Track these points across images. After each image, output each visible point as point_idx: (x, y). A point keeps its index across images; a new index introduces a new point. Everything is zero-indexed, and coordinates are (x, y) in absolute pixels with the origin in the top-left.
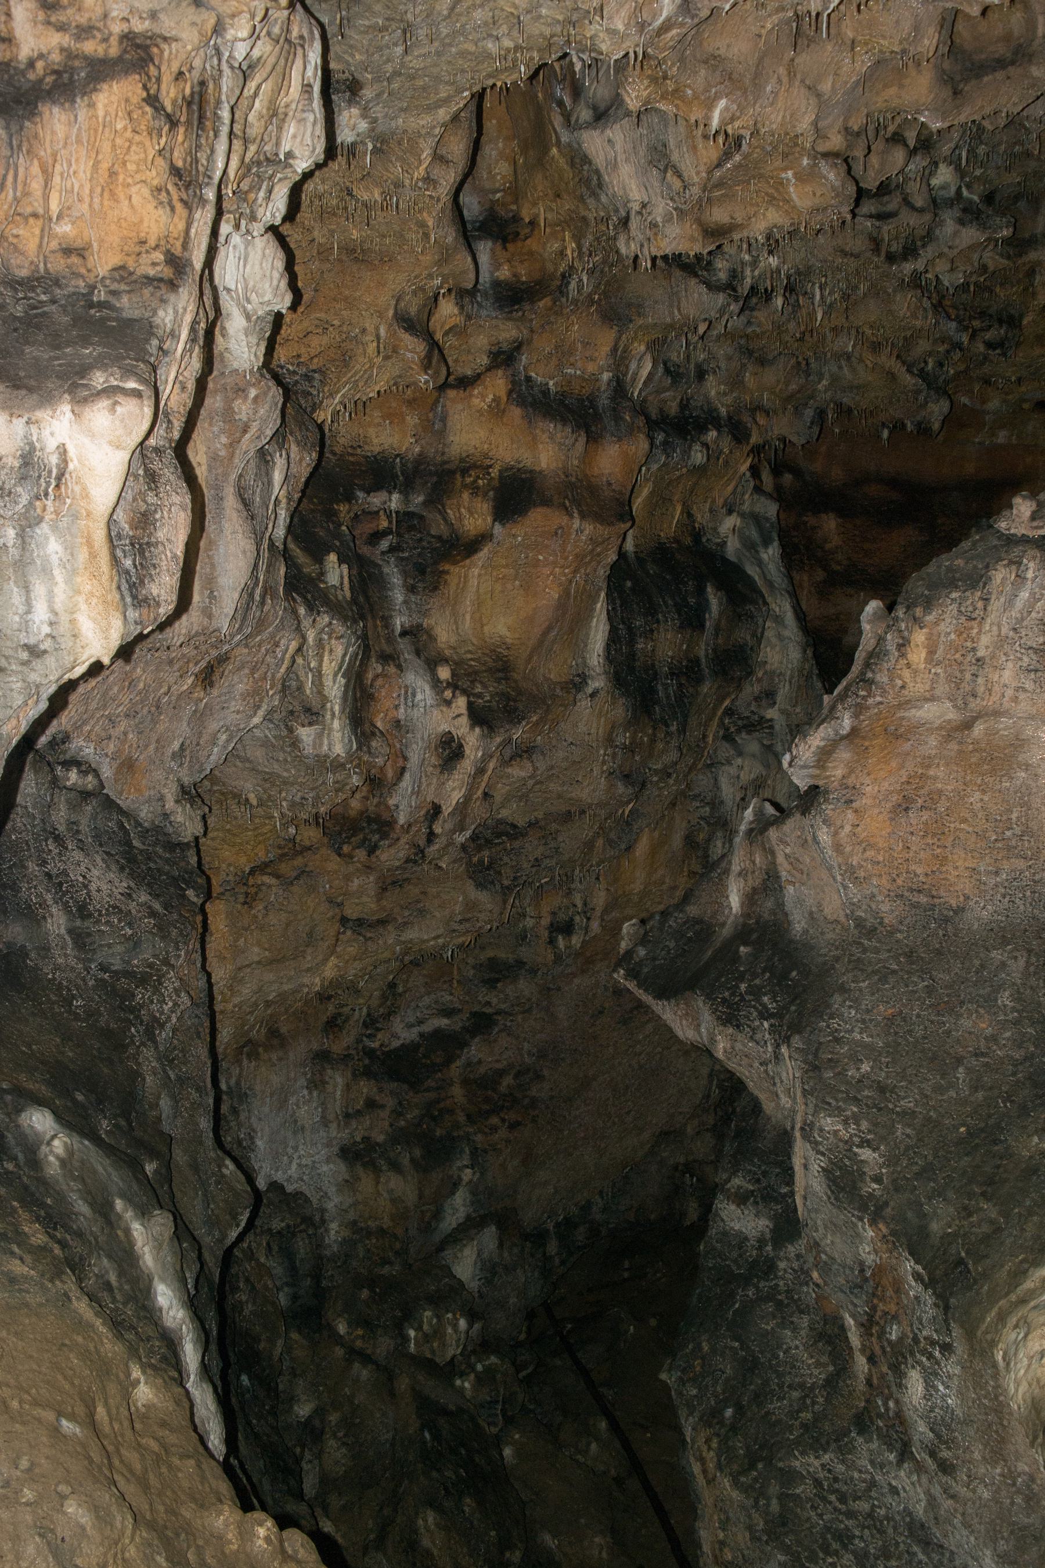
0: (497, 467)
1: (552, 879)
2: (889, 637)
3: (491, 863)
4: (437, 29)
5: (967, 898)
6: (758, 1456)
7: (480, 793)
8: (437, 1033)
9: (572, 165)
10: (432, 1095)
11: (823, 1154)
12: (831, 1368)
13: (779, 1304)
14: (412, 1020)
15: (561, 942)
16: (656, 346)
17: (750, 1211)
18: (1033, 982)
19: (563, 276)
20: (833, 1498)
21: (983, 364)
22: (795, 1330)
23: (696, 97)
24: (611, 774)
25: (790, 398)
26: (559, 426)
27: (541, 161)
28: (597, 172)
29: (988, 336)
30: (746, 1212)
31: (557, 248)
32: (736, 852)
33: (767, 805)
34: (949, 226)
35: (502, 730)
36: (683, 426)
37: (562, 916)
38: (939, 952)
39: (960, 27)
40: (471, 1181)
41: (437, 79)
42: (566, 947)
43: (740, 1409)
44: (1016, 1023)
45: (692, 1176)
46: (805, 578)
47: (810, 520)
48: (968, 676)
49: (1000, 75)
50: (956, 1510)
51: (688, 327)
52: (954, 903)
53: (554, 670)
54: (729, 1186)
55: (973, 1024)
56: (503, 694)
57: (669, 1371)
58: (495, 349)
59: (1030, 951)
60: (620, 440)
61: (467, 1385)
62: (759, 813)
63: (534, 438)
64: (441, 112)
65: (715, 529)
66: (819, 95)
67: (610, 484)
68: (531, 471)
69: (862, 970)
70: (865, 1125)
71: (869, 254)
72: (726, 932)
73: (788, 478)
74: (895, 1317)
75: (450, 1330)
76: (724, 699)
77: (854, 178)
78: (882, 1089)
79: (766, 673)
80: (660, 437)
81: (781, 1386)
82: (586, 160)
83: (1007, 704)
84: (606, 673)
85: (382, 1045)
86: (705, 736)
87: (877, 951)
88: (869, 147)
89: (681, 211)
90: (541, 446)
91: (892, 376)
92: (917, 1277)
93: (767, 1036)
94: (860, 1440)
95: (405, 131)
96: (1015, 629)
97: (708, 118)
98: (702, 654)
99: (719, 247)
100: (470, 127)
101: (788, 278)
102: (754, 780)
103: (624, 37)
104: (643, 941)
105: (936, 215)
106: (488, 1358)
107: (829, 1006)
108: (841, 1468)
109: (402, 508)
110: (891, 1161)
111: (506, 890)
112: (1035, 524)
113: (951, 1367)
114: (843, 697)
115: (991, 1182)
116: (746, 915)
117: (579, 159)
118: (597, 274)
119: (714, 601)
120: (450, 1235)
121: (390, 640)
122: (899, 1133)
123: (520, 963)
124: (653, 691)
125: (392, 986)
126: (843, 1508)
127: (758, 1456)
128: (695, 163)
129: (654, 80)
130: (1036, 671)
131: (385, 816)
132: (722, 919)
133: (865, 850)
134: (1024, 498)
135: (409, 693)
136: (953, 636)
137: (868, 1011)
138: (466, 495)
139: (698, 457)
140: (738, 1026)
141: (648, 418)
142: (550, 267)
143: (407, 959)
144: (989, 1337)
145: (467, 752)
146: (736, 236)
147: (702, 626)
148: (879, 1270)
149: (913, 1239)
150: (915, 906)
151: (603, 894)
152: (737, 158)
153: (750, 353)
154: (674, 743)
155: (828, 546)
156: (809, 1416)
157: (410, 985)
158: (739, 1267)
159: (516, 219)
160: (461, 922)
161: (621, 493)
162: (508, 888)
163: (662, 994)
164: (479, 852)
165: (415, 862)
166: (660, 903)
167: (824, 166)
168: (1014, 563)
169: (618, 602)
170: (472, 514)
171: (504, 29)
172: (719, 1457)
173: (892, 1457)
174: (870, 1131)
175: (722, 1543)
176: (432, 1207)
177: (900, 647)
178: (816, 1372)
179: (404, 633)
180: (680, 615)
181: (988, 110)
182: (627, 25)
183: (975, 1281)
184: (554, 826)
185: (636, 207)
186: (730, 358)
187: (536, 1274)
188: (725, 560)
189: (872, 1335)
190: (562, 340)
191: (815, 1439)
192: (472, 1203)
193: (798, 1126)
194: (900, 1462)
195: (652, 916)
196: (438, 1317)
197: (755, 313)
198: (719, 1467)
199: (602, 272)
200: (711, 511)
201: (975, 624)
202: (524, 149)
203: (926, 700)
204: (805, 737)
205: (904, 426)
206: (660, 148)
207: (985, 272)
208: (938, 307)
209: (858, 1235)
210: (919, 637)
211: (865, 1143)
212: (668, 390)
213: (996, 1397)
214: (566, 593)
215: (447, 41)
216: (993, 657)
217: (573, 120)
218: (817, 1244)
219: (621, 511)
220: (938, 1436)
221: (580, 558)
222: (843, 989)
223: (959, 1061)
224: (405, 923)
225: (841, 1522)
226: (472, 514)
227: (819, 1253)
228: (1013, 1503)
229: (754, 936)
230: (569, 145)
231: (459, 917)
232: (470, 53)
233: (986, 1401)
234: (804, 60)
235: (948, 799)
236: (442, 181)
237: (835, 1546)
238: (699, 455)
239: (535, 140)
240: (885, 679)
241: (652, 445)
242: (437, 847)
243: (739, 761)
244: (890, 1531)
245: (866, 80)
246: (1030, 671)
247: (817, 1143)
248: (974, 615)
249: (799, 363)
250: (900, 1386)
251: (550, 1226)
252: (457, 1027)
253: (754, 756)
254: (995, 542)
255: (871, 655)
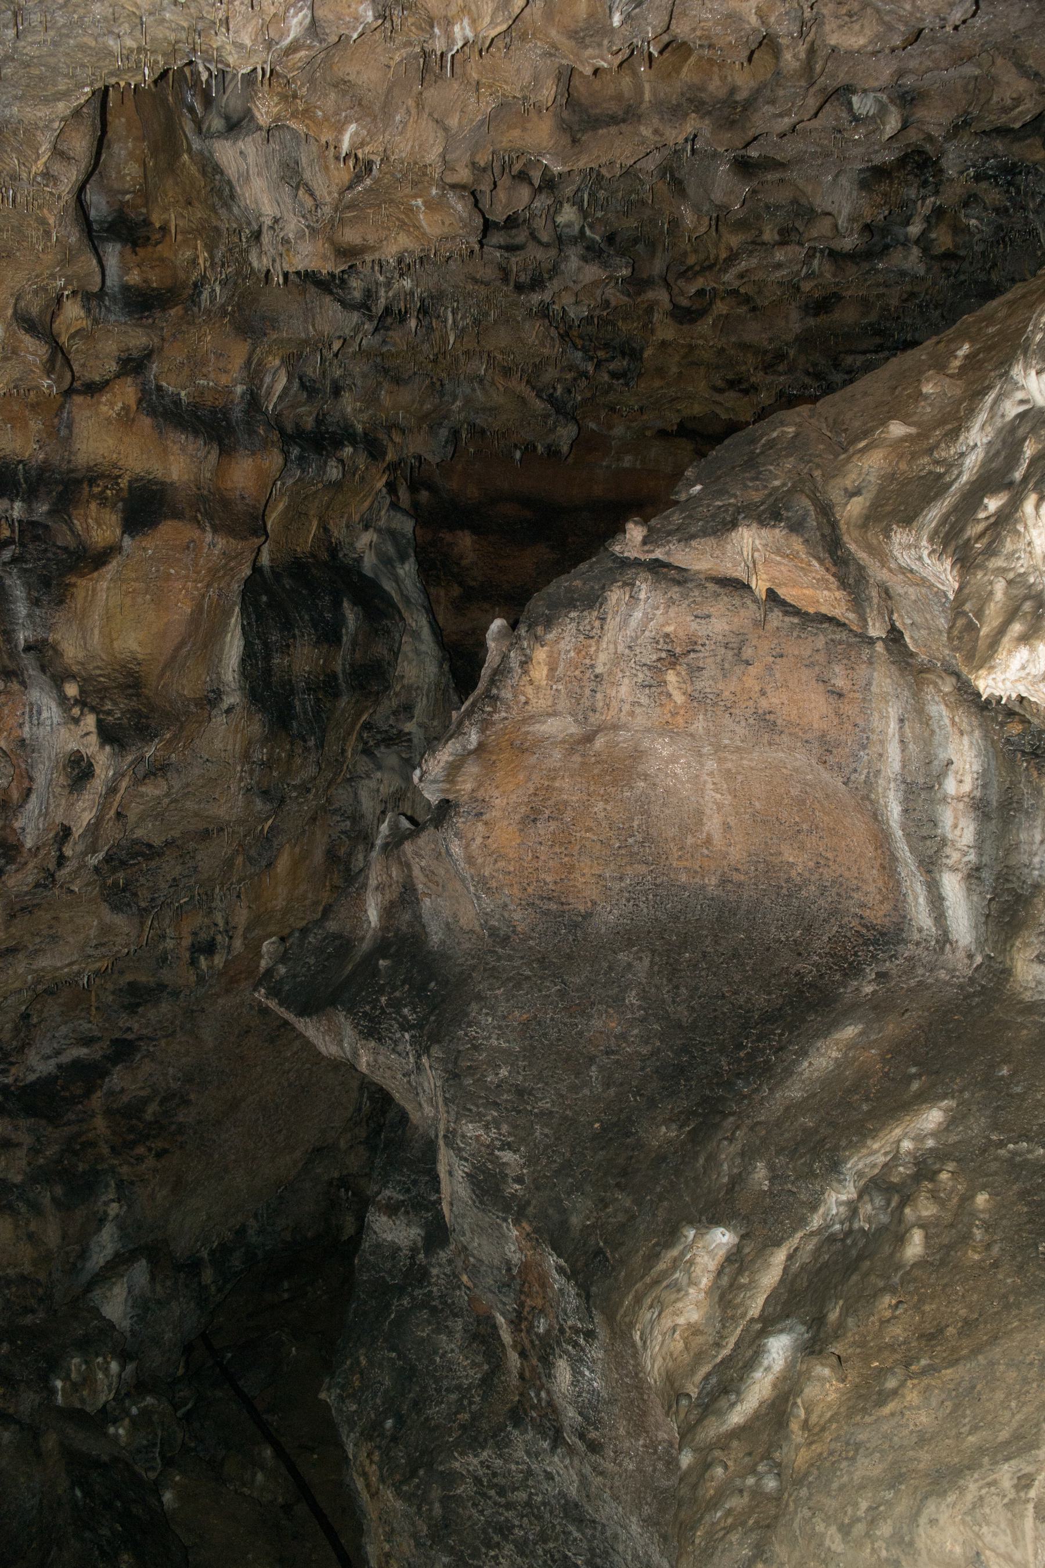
0: (127, 478)
1: (192, 898)
2: (512, 654)
3: (126, 885)
4: (53, 18)
5: (594, 903)
6: (417, 1465)
7: (112, 813)
8: (76, 1063)
9: (204, 173)
10: (74, 1128)
11: (466, 1160)
12: (486, 1367)
13: (434, 1310)
14: (49, 1051)
15: (203, 962)
16: (292, 361)
17: (401, 1220)
18: (657, 980)
19: (195, 285)
20: (492, 1493)
21: (607, 392)
22: (450, 1333)
23: (326, 119)
24: (248, 790)
25: (427, 415)
26: (191, 438)
27: (172, 167)
28: (229, 183)
29: (612, 366)
30: (398, 1222)
31: (189, 256)
32: (373, 867)
33: (402, 818)
34: (574, 262)
35: (134, 748)
36: (318, 441)
37: (203, 936)
38: (569, 957)
39: (576, 81)
40: (117, 1216)
41: (55, 70)
42: (210, 968)
43: (400, 1420)
44: (643, 1020)
45: (347, 1191)
46: (442, 593)
47: (448, 537)
48: (587, 692)
49: (613, 130)
50: (605, 1485)
51: (321, 344)
52: (582, 909)
53: (188, 685)
54: (379, 1197)
55: (604, 1023)
56: (135, 711)
57: (328, 1390)
58: (124, 356)
59: (653, 952)
60: (254, 453)
61: (121, 1431)
62: (395, 827)
63: (165, 450)
64: (61, 105)
65: (352, 544)
66: (446, 129)
67: (243, 498)
68: (163, 483)
69: (497, 978)
70: (505, 1128)
71: (498, 283)
72: (365, 946)
73: (424, 495)
74: (541, 1311)
75: (100, 1375)
76: (360, 716)
77: (480, 210)
78: (520, 1092)
79: (403, 687)
80: (295, 452)
81: (438, 1391)
82: (218, 170)
83: (624, 718)
84: (241, 688)
85: (16, 1080)
86: (343, 751)
87: (510, 958)
88: (495, 183)
89: (313, 229)
90: (172, 458)
91: (523, 400)
92: (560, 1270)
93: (409, 1047)
94: (516, 1433)
95: (20, 121)
96: (630, 647)
97: (338, 141)
98: (339, 669)
99: (350, 267)
100: (93, 124)
101: (422, 301)
102: (394, 793)
103: (251, 53)
104: (283, 959)
105: (560, 250)
106: (144, 1399)
107: (467, 1015)
108: (499, 1462)
109: (25, 517)
110: (531, 1160)
111: (143, 912)
112: (646, 548)
113: (596, 1352)
114: (469, 713)
115: (624, 1173)
116: (385, 928)
117: (211, 169)
118: (230, 285)
119: (351, 616)
120: (97, 1275)
121: (12, 655)
122: (537, 1134)
123: (162, 987)
124: (291, 707)
125: (26, 1016)
126: (503, 1500)
127: (417, 1465)
128: (327, 183)
129: (284, 98)
130: (650, 686)
131: (12, 840)
132: (361, 934)
133: (496, 861)
134: (636, 523)
135: (34, 711)
136: (572, 654)
137: (504, 1017)
138: (93, 506)
139: (334, 472)
140: (380, 1039)
141: (282, 432)
142: (182, 275)
143: (40, 988)
144: (627, 1319)
145: (98, 771)
146: (368, 258)
147: (339, 640)
148: (525, 1267)
149: (553, 1234)
150: (546, 913)
151: (245, 912)
152: (368, 182)
153: (386, 371)
154: (313, 757)
155: (464, 562)
156: (467, 1416)
157: (45, 1015)
158: (393, 1279)
159: (147, 223)
160: (96, 947)
161: (254, 507)
162: (144, 909)
163: (305, 1010)
164: (113, 873)
165: (45, 886)
166: (303, 919)
167: (452, 197)
168: (628, 584)
169: (253, 616)
170: (100, 526)
171: (126, 27)
172: (381, 1469)
173: (546, 1445)
174: (510, 1134)
175: (388, 1555)
176: (77, 1247)
177: (523, 664)
178: (471, 1372)
179: (28, 648)
180: (316, 630)
181: (603, 160)
182: (254, 41)
183: (613, 1269)
184: (192, 845)
185: (268, 222)
186: (364, 376)
187: (192, 1305)
188: (362, 576)
189: (521, 1331)
190: (195, 350)
191: (473, 1441)
192: (121, 1238)
193: (441, 1134)
194: (554, 1448)
195: (290, 934)
196: (86, 1362)
197: (390, 333)
198: (382, 1479)
199: (235, 284)
200: (347, 527)
201: (592, 642)
202: (155, 152)
203: (549, 715)
204: (434, 752)
205: (535, 448)
206: (292, 165)
207: (608, 307)
208: (564, 337)
209: (503, 1235)
210: (541, 654)
211: (506, 1146)
212: (304, 405)
213: (637, 1374)
214: (199, 609)
215: (64, 31)
216: (610, 674)
217: (204, 128)
218: (465, 1248)
219: (254, 525)
220: (586, 1418)
221: (213, 572)
222: (479, 997)
223: (592, 1060)
224: (37, 951)
225: (501, 1514)
226: (100, 526)
227: (467, 1256)
228: (654, 1471)
229: (393, 950)
230: (201, 153)
231: (95, 942)
232: (90, 48)
233: (627, 1380)
234: (432, 94)
235: (574, 809)
236: (63, 178)
237: (497, 1538)
238: (335, 470)
239: (166, 144)
240: (509, 696)
241: (286, 460)
242: (68, 870)
243: (379, 775)
244: (547, 1515)
245: (490, 121)
246: (644, 687)
247: (460, 1149)
248: (592, 634)
249: (433, 383)
250: (549, 1376)
251: (205, 1254)
252: (98, 1056)
253: (393, 769)
254: (611, 565)
255: (496, 672)
